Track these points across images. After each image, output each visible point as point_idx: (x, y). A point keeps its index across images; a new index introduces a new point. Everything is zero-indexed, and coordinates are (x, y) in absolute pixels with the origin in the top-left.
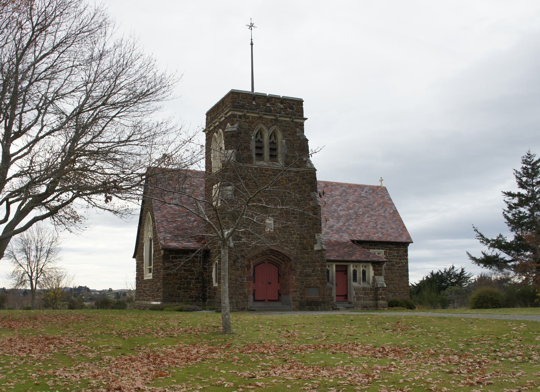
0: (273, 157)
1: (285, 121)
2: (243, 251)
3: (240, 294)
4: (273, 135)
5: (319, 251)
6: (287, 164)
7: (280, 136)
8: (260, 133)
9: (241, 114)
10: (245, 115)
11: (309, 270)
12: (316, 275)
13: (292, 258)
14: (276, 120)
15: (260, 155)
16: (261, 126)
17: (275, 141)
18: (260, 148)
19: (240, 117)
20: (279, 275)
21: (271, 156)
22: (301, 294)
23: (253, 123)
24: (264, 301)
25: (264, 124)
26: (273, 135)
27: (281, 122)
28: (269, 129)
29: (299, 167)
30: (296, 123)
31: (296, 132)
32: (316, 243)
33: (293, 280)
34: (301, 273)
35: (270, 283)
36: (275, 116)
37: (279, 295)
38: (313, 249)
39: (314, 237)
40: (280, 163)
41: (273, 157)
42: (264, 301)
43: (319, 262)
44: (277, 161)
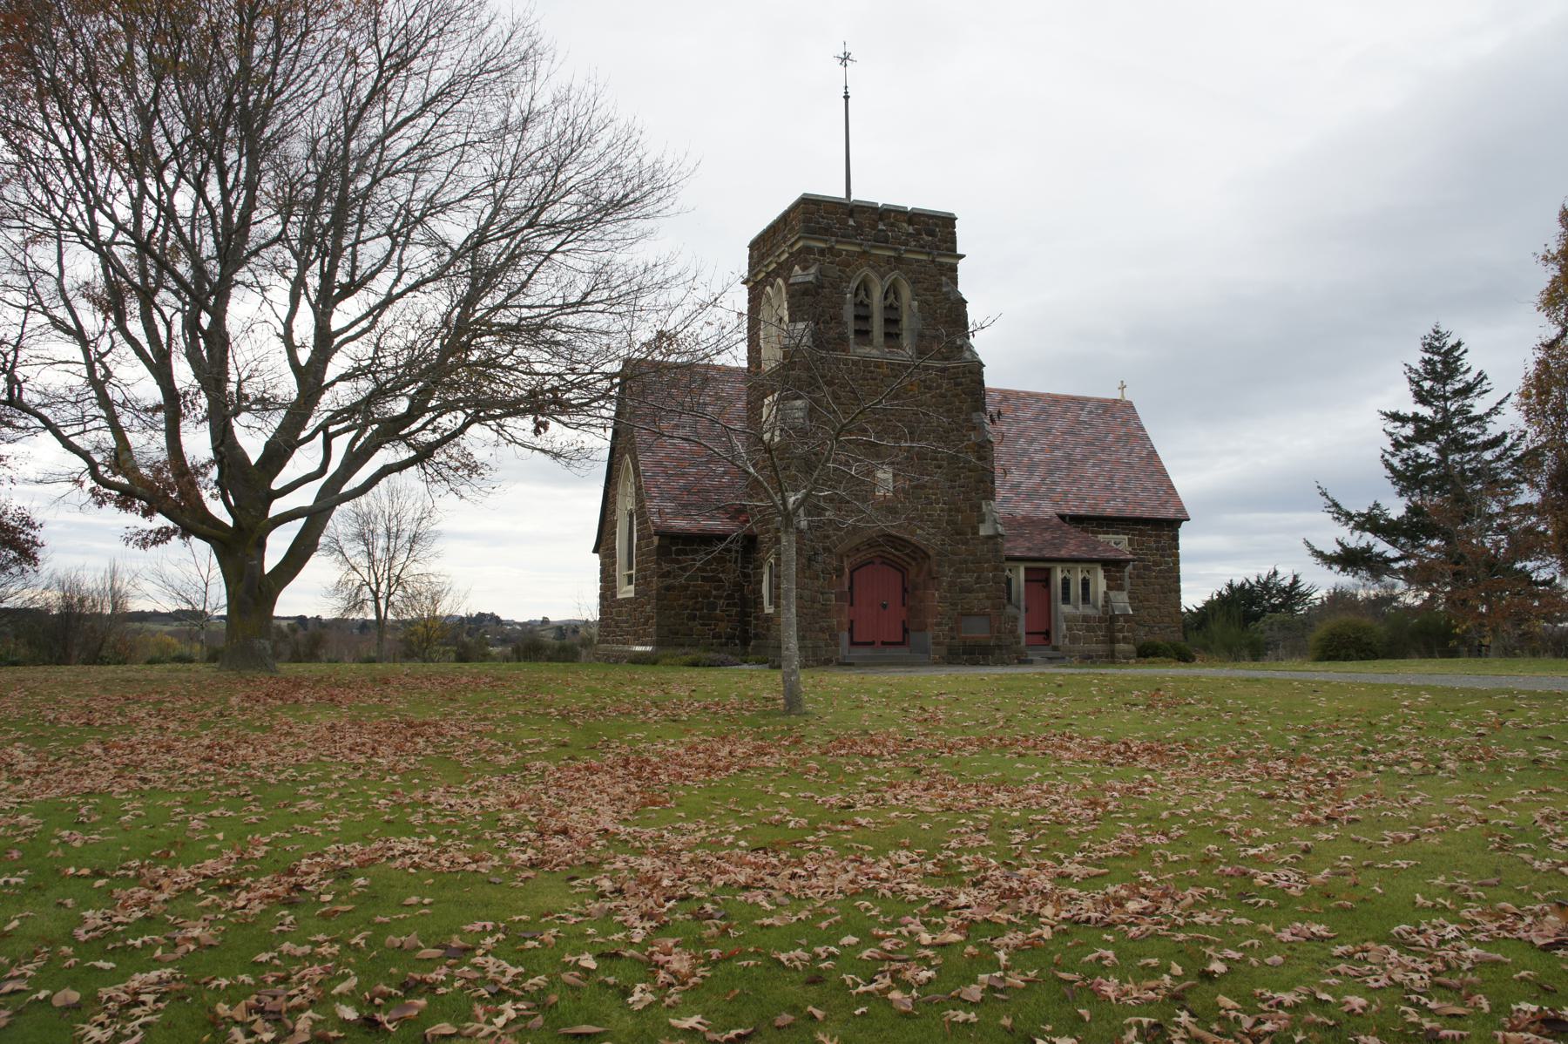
0: (892, 337)
1: (917, 261)
2: (828, 537)
3: (822, 630)
4: (892, 290)
5: (989, 537)
6: (921, 352)
7: (906, 292)
8: (865, 286)
9: (822, 245)
10: (831, 249)
11: (968, 579)
12: (982, 590)
13: (931, 553)
14: (899, 259)
15: (863, 334)
16: (866, 271)
17: (896, 304)
18: (863, 317)
19: (822, 252)
20: (905, 590)
21: (888, 335)
22: (951, 629)
23: (848, 265)
24: (872, 643)
25: (872, 267)
26: (892, 290)
27: (910, 262)
28: (882, 278)
29: (947, 359)
30: (941, 264)
31: (940, 285)
32: (983, 521)
33: (935, 598)
34: (952, 584)
35: (884, 607)
36: (895, 250)
37: (905, 631)
38: (977, 533)
39: (980, 507)
40: (906, 351)
41: (892, 337)
42: (872, 643)
43: (988, 561)
44: (900, 347)
